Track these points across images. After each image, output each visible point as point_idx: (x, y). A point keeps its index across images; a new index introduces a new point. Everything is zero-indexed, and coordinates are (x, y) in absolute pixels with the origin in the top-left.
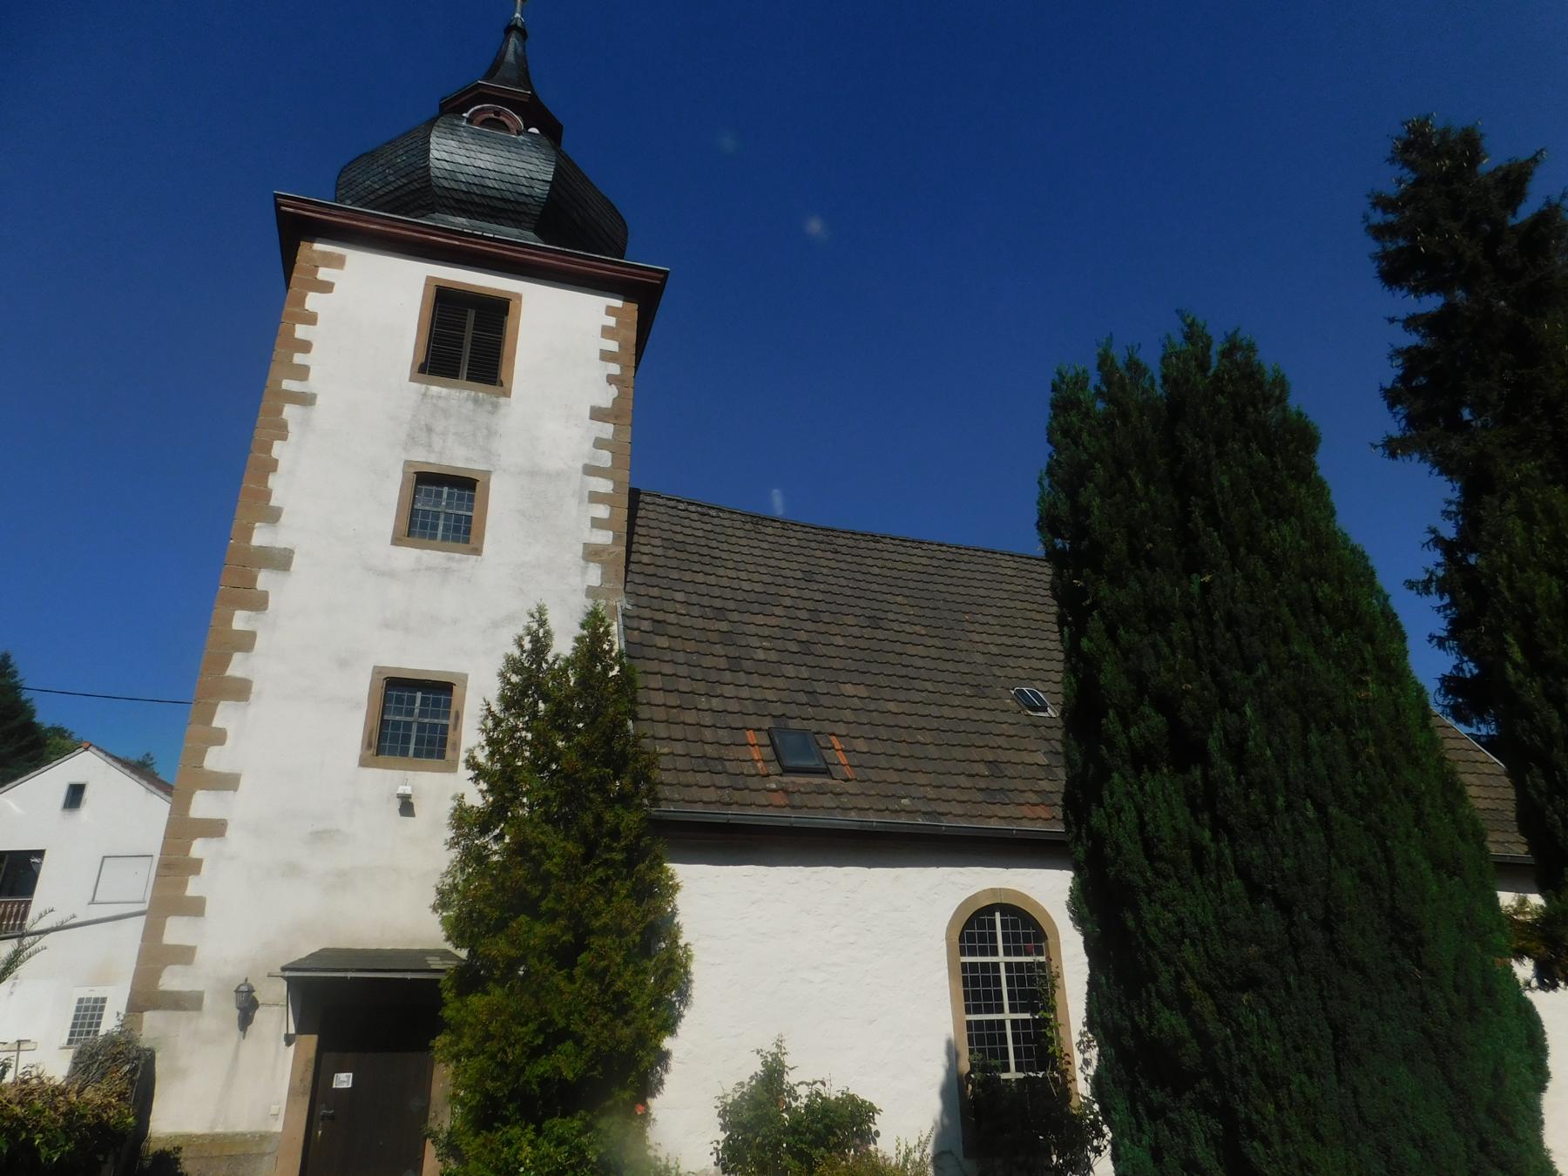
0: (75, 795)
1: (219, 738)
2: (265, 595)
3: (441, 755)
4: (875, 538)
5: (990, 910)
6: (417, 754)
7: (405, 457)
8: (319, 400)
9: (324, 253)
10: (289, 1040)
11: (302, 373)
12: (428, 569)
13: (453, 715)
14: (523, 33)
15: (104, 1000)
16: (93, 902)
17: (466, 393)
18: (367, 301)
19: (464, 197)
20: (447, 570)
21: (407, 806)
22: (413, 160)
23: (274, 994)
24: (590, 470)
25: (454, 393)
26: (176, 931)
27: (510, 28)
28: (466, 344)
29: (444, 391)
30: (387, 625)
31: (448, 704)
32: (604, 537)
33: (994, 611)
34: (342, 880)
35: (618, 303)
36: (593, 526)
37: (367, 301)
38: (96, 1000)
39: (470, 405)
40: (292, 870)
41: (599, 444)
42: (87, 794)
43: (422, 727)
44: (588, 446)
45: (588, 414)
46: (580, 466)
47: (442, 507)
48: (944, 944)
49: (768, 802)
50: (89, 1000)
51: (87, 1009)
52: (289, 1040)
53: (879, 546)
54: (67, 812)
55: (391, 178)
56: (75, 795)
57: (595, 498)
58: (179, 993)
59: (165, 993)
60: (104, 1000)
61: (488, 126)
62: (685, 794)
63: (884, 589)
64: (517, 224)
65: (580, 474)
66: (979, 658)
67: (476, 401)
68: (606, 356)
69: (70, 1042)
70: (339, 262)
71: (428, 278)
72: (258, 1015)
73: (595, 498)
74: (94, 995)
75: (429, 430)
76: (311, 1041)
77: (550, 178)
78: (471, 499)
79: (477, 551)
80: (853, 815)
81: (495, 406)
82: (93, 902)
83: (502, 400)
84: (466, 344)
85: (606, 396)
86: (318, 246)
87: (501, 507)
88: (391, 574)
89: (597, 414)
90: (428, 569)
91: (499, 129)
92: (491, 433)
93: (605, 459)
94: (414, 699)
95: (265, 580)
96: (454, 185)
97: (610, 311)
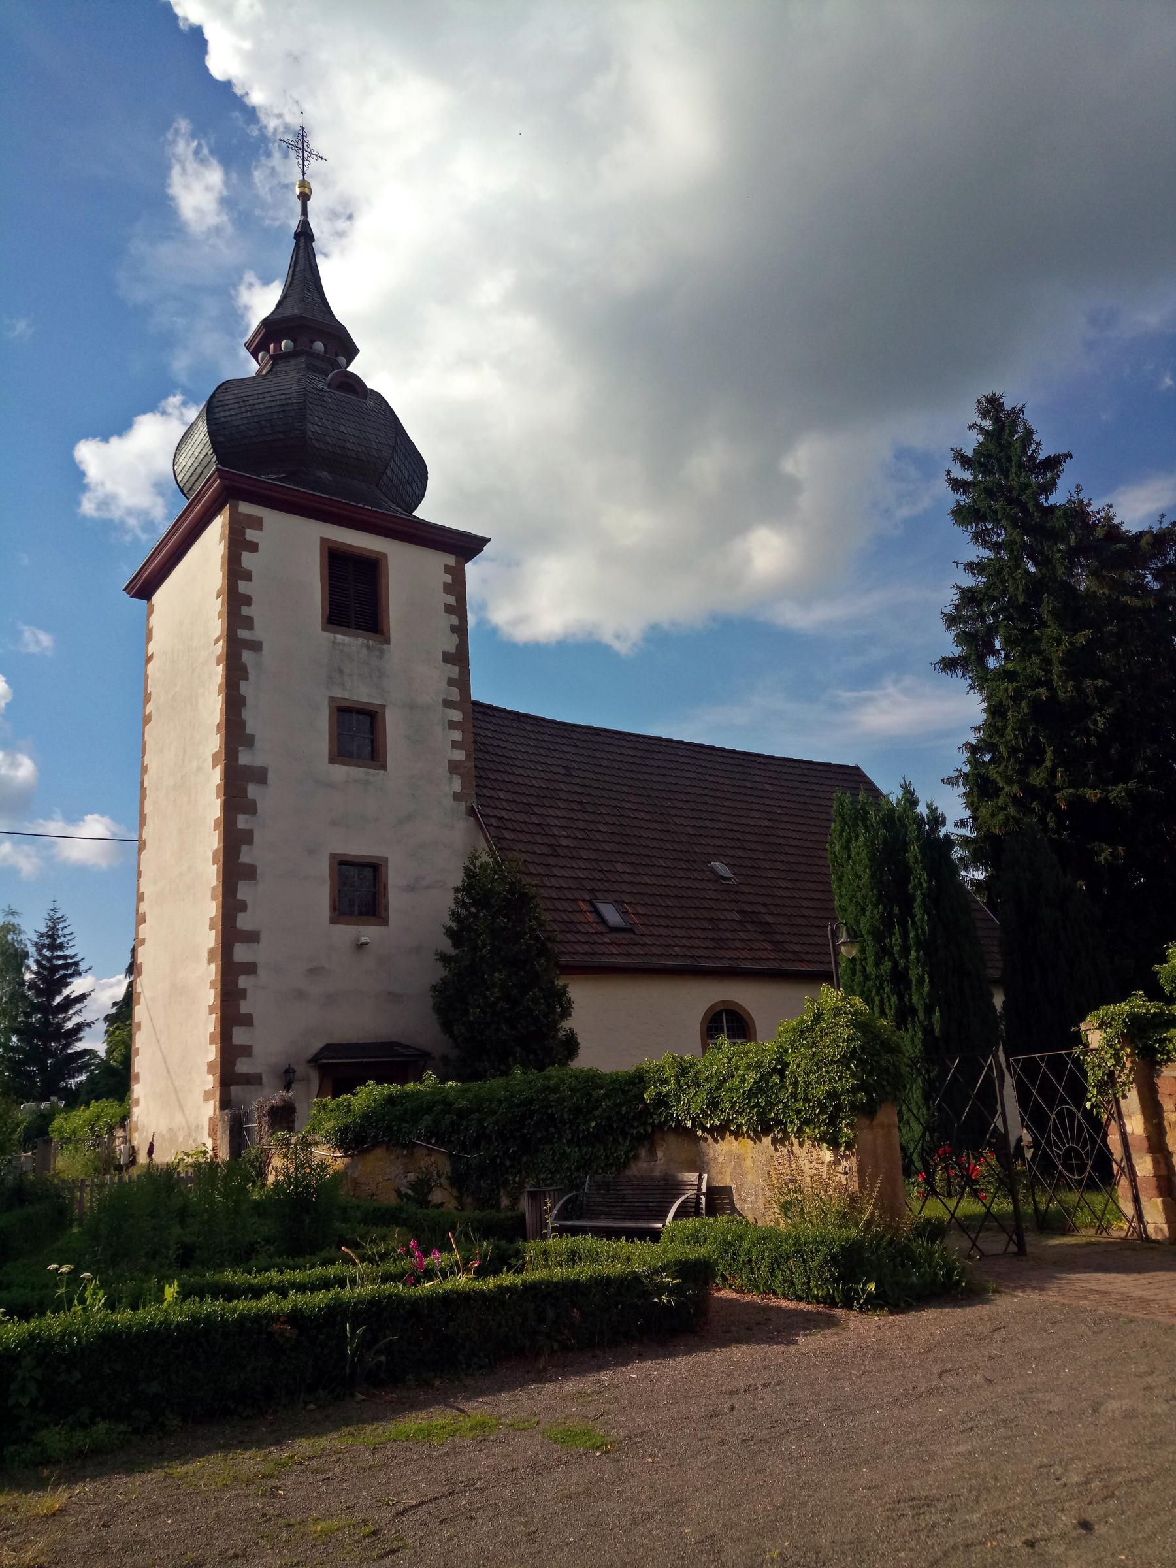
5: (719, 1013)
8: (265, 646)
12: (356, 781)
17: (360, 641)
20: (367, 782)
29: (346, 639)
33: (682, 797)
39: (364, 651)
40: (300, 995)
55: (268, 431)
57: (452, 725)
58: (247, 1074)
65: (441, 707)
66: (684, 839)
67: (368, 647)
73: (452, 725)
75: (341, 672)
79: (383, 767)
81: (382, 651)
83: (385, 647)
88: (332, 786)
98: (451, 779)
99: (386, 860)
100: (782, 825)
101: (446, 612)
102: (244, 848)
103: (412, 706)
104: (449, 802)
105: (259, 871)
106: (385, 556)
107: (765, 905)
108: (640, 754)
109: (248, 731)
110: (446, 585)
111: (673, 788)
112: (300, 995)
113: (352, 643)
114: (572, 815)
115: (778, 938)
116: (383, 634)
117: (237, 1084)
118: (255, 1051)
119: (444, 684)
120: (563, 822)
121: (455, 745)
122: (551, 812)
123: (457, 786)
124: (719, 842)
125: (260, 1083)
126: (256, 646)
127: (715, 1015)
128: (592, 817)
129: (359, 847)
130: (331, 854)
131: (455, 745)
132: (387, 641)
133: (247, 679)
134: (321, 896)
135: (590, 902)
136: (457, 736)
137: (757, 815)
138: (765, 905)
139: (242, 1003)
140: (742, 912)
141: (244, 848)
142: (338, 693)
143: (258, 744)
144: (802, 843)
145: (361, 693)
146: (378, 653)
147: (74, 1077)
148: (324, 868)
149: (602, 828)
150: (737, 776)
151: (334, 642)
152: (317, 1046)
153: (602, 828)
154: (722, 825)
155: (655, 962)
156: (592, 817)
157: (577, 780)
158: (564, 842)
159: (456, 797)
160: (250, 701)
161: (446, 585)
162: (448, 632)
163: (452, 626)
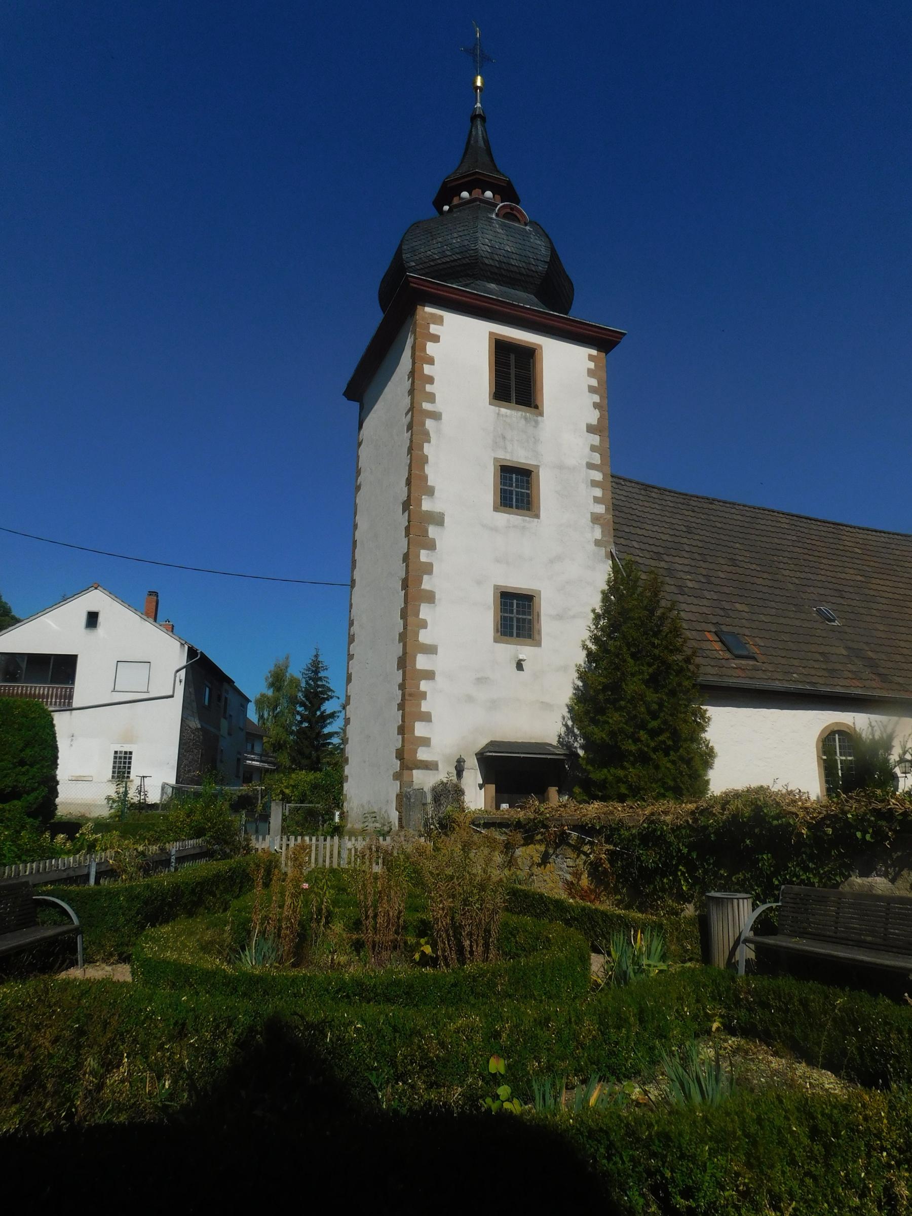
0: (92, 619)
1: (424, 625)
2: (433, 541)
3: (530, 636)
4: (712, 501)
5: (833, 733)
6: (518, 635)
7: (493, 455)
8: (444, 416)
9: (431, 314)
10: (481, 787)
11: (431, 398)
12: (514, 526)
13: (535, 614)
14: (483, 119)
15: (131, 753)
16: (114, 691)
17: (520, 413)
18: (458, 346)
19: (496, 270)
20: (524, 528)
21: (520, 666)
22: (466, 243)
23: (472, 763)
24: (590, 466)
25: (514, 413)
26: (420, 729)
27: (474, 118)
28: (514, 378)
29: (508, 412)
30: (498, 561)
31: (529, 607)
32: (600, 509)
33: (786, 554)
34: (493, 705)
35: (594, 352)
36: (595, 502)
37: (458, 346)
38: (126, 753)
39: (523, 422)
40: (470, 699)
41: (593, 448)
42: (101, 619)
43: (518, 619)
44: (587, 450)
45: (585, 429)
46: (584, 463)
47: (516, 488)
48: (815, 749)
49: (736, 673)
50: (121, 752)
51: (120, 758)
52: (481, 787)
53: (714, 507)
54: (88, 631)
55: (448, 253)
56: (92, 619)
57: (594, 484)
58: (427, 761)
59: (421, 761)
60: (131, 753)
61: (508, 219)
62: (709, 673)
63: (727, 538)
64: (526, 290)
65: (585, 469)
66: (791, 587)
67: (526, 419)
68: (592, 390)
69: (113, 777)
70: (440, 321)
71: (491, 334)
72: (465, 773)
73: (594, 484)
74: (124, 750)
75: (504, 438)
76: (492, 788)
77: (548, 259)
78: (528, 482)
79: (537, 516)
80: (777, 683)
81: (537, 422)
82: (114, 691)
83: (540, 418)
84: (514, 378)
85: (593, 417)
86: (428, 309)
87: (547, 487)
88: (494, 529)
89: (590, 429)
90: (514, 526)
91: (513, 220)
92: (536, 441)
93: (597, 459)
94: (513, 603)
95: (432, 531)
96: (491, 262)
97: (591, 358)
98: (593, 528)
99: (496, 509)
100: (874, 581)
101: (590, 391)
102: (425, 577)
103: (561, 467)
104: (592, 547)
105: (437, 597)
106: (540, 347)
107: (867, 643)
108: (748, 519)
109: (429, 484)
110: (589, 371)
111: (778, 547)
112: (470, 699)
113: (512, 414)
114: (693, 563)
115: (882, 671)
116: (536, 407)
117: (418, 768)
118: (433, 742)
119: (587, 450)
120: (686, 569)
121: (596, 500)
122: (677, 559)
123: (598, 533)
124: (822, 591)
125: (437, 769)
126: (436, 416)
127: (829, 734)
128: (712, 566)
129: (518, 582)
130: (495, 586)
131: (596, 500)
132: (541, 414)
133: (429, 442)
134: (486, 618)
135: (716, 633)
136: (598, 492)
137: (852, 571)
138: (867, 643)
139: (423, 703)
140: (848, 648)
141: (426, 578)
142: (501, 455)
143: (437, 493)
144: (890, 595)
145: (520, 457)
146: (533, 423)
147: (616, 768)
148: (489, 598)
149: (722, 575)
150: (831, 540)
151: (498, 414)
152: (482, 742)
153: (722, 575)
154: (823, 578)
155: (777, 685)
156: (712, 566)
157: (697, 537)
158: (690, 584)
159: (597, 543)
160: (431, 459)
161: (589, 371)
162: (592, 408)
163: (594, 403)
